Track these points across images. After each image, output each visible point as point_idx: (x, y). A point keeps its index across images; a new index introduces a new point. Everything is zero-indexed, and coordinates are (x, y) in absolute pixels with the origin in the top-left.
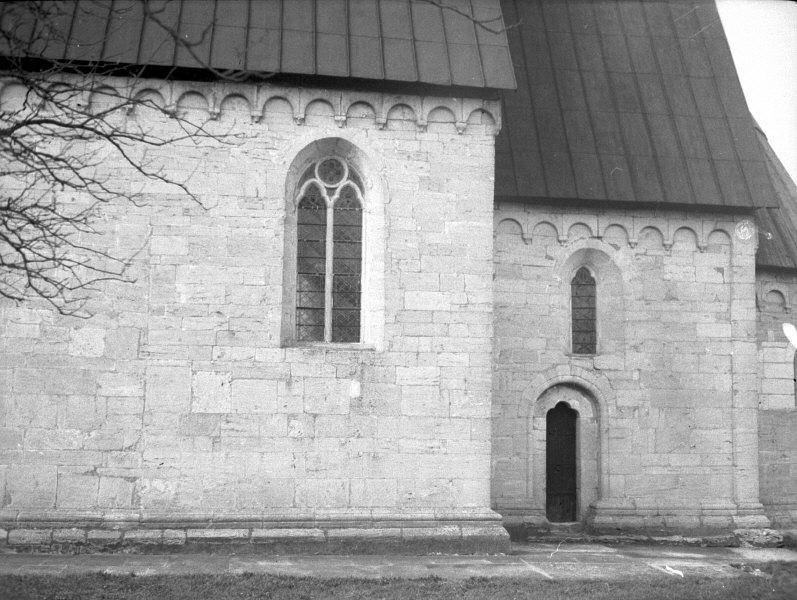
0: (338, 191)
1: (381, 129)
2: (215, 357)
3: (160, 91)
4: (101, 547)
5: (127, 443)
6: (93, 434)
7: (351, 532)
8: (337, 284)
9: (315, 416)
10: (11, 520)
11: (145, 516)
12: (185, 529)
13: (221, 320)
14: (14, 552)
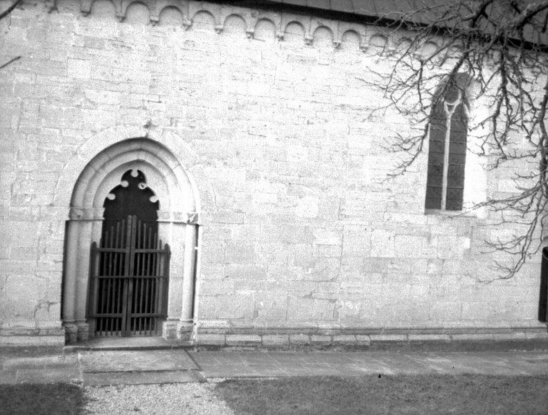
0: (454, 108)
1: (308, 44)
2: (386, 220)
3: (244, 17)
4: (320, 347)
5: (331, 276)
6: (310, 270)
7: (465, 337)
8: (450, 171)
9: (444, 261)
10: (261, 329)
11: (344, 326)
12: (368, 335)
13: (389, 194)
14: (266, 351)
